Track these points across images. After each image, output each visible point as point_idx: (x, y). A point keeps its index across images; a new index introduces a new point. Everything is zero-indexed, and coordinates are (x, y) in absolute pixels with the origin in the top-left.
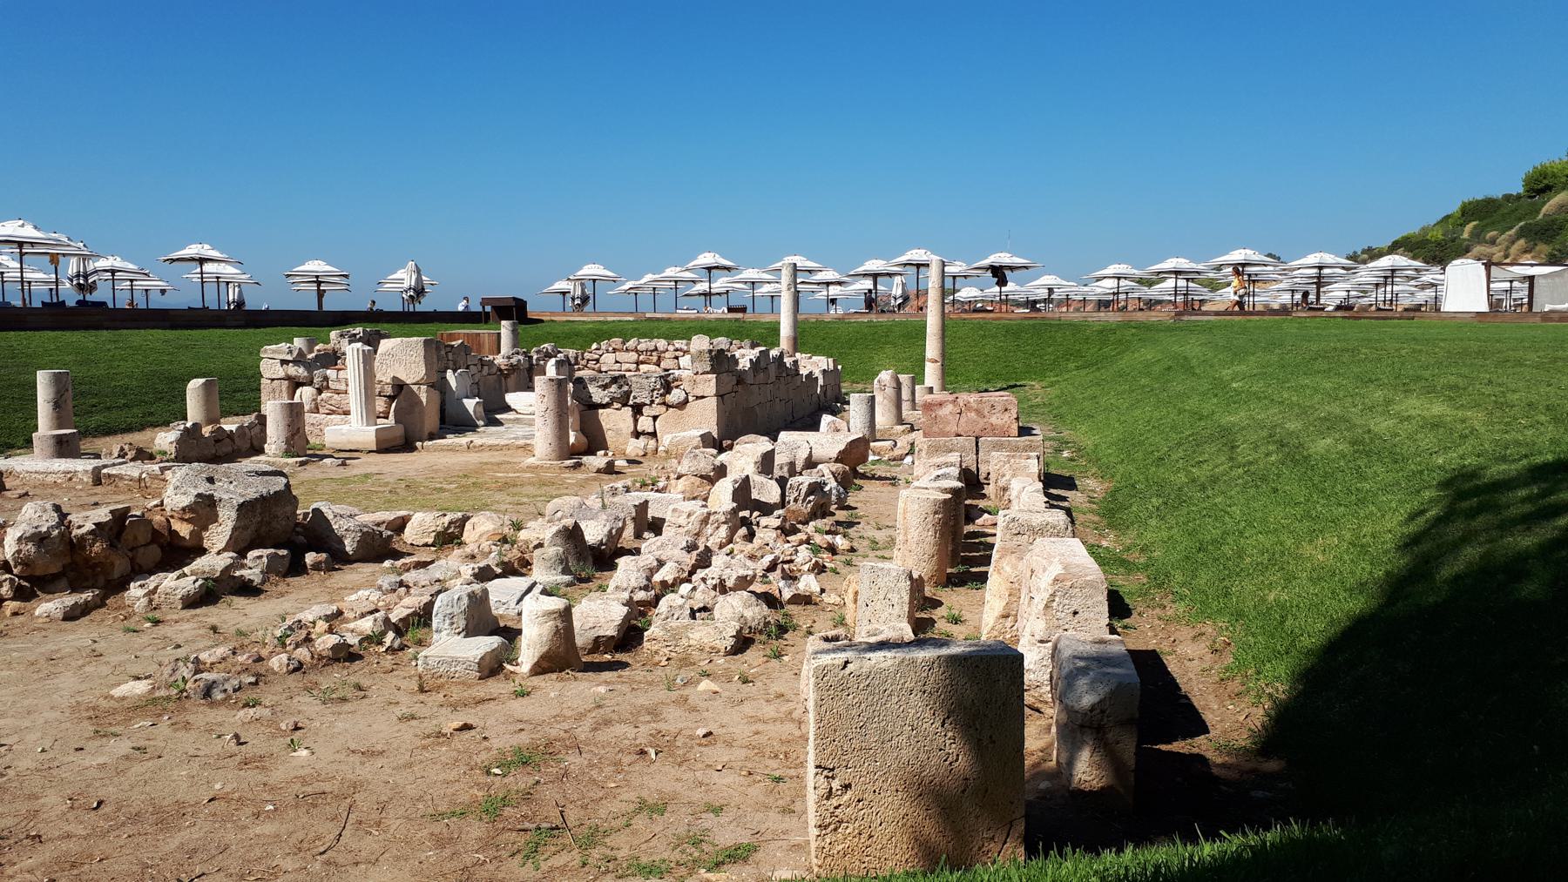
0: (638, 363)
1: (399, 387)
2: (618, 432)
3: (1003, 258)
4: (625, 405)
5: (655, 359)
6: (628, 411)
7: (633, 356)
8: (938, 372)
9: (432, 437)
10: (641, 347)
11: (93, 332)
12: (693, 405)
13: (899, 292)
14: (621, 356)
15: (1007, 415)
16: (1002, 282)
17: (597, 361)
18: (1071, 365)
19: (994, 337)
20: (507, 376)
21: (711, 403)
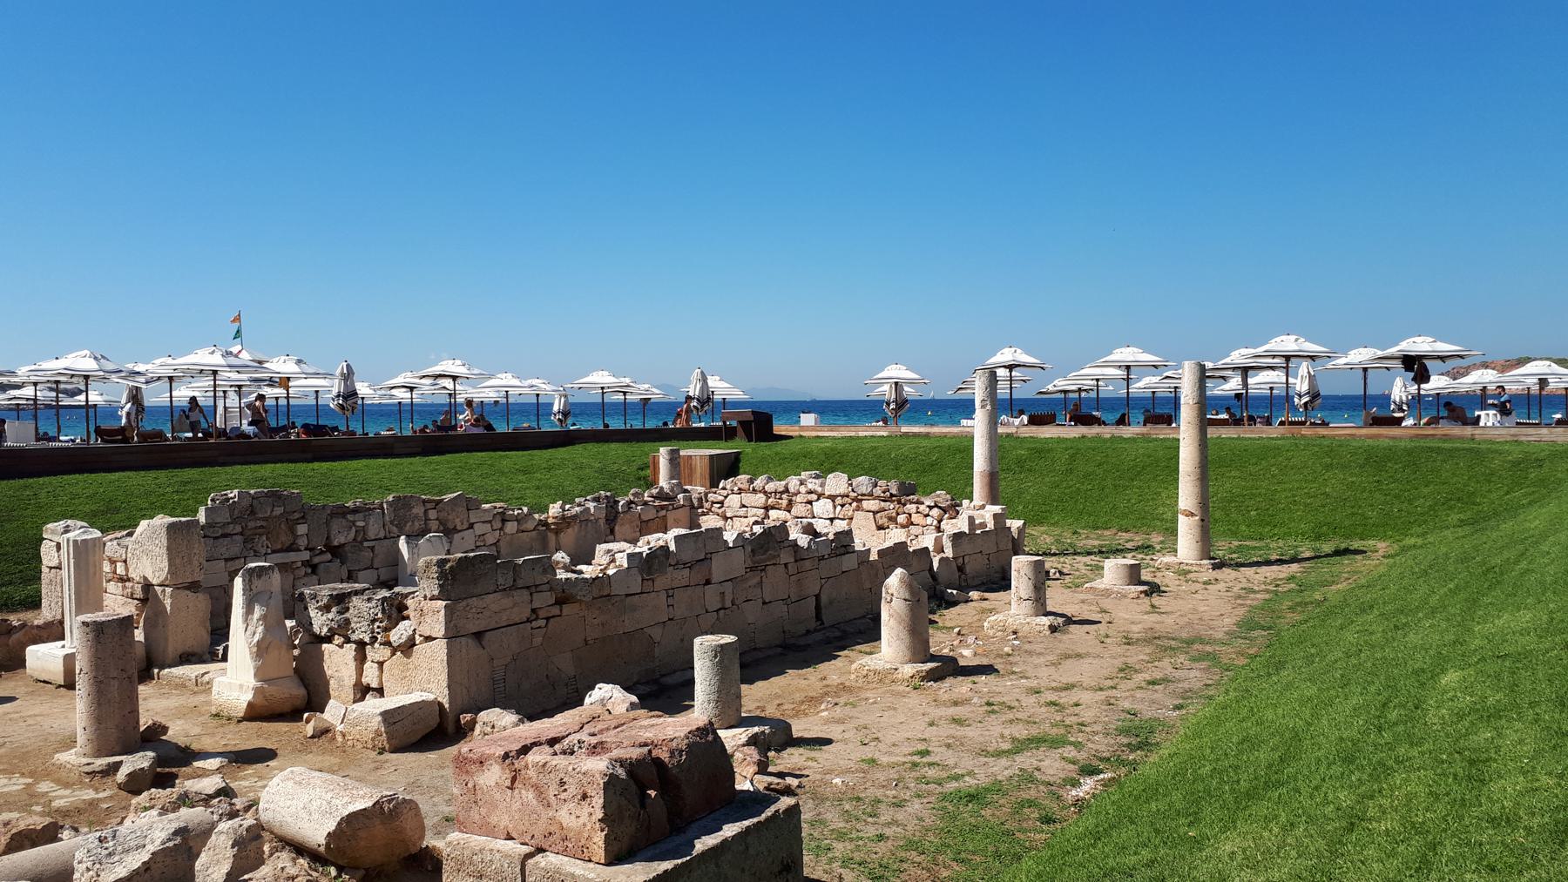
0: (767, 508)
1: (147, 586)
2: (340, 680)
3: (1419, 345)
4: (348, 641)
5: (784, 502)
6: (350, 649)
7: (760, 499)
8: (1196, 531)
9: (187, 658)
10: (770, 487)
11: (143, 473)
12: (421, 648)
13: (1305, 388)
14: (749, 499)
15: (586, 810)
16: (1422, 376)
17: (722, 503)
18: (1454, 517)
19: (1344, 467)
20: (557, 532)
21: (439, 649)
